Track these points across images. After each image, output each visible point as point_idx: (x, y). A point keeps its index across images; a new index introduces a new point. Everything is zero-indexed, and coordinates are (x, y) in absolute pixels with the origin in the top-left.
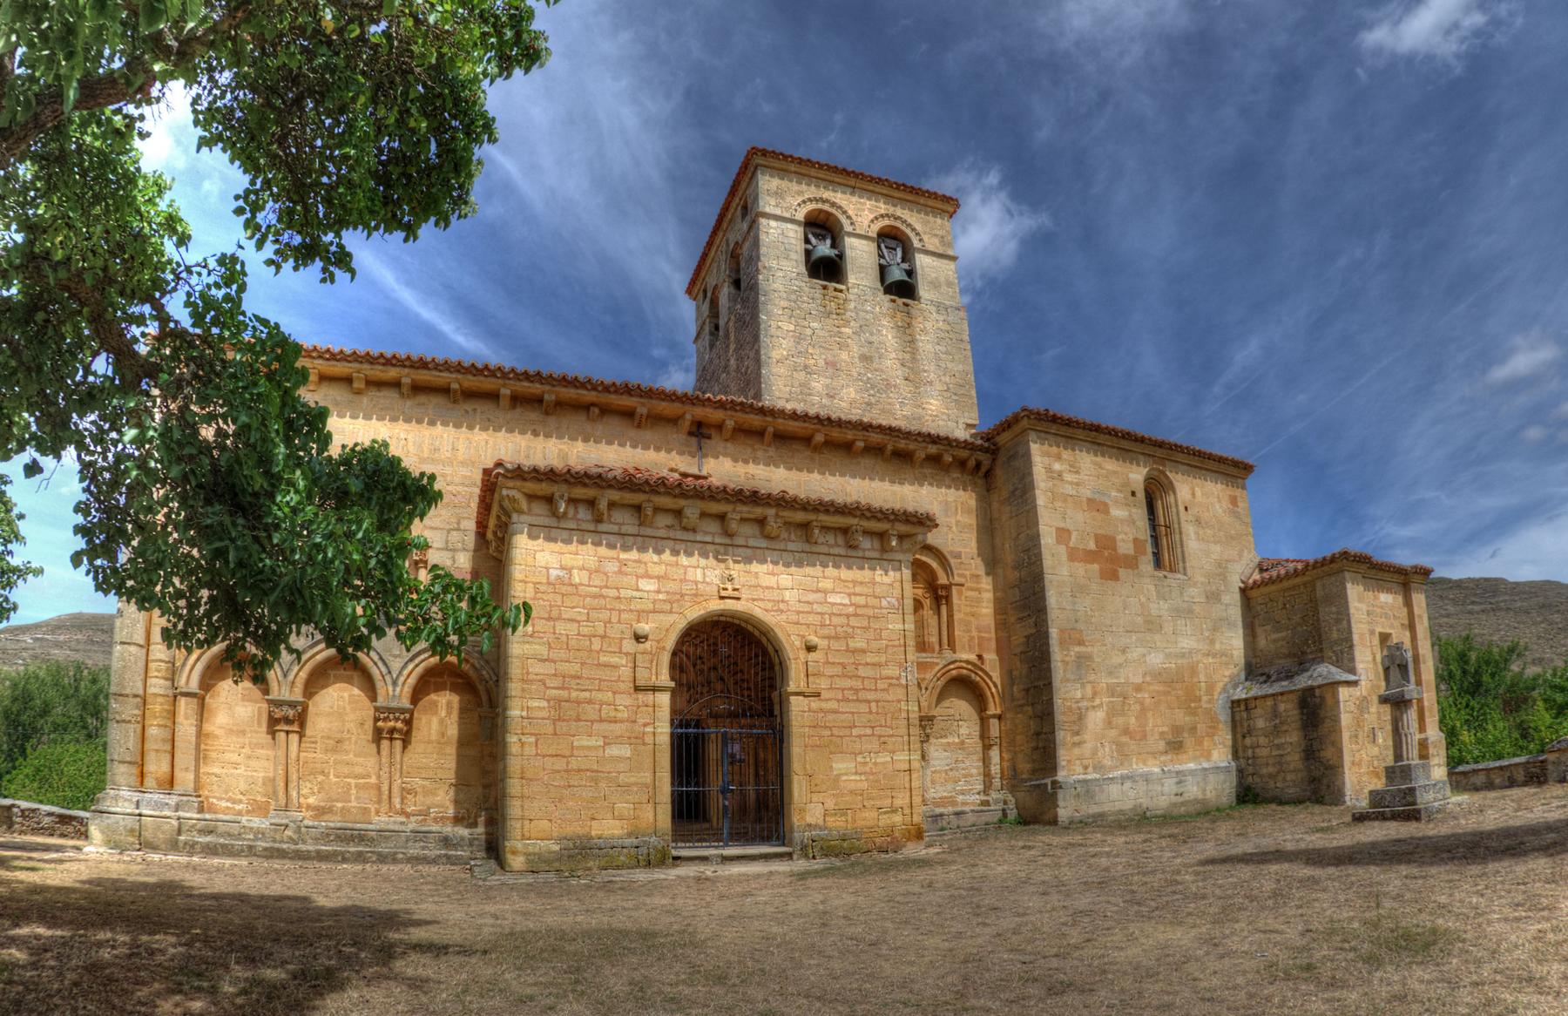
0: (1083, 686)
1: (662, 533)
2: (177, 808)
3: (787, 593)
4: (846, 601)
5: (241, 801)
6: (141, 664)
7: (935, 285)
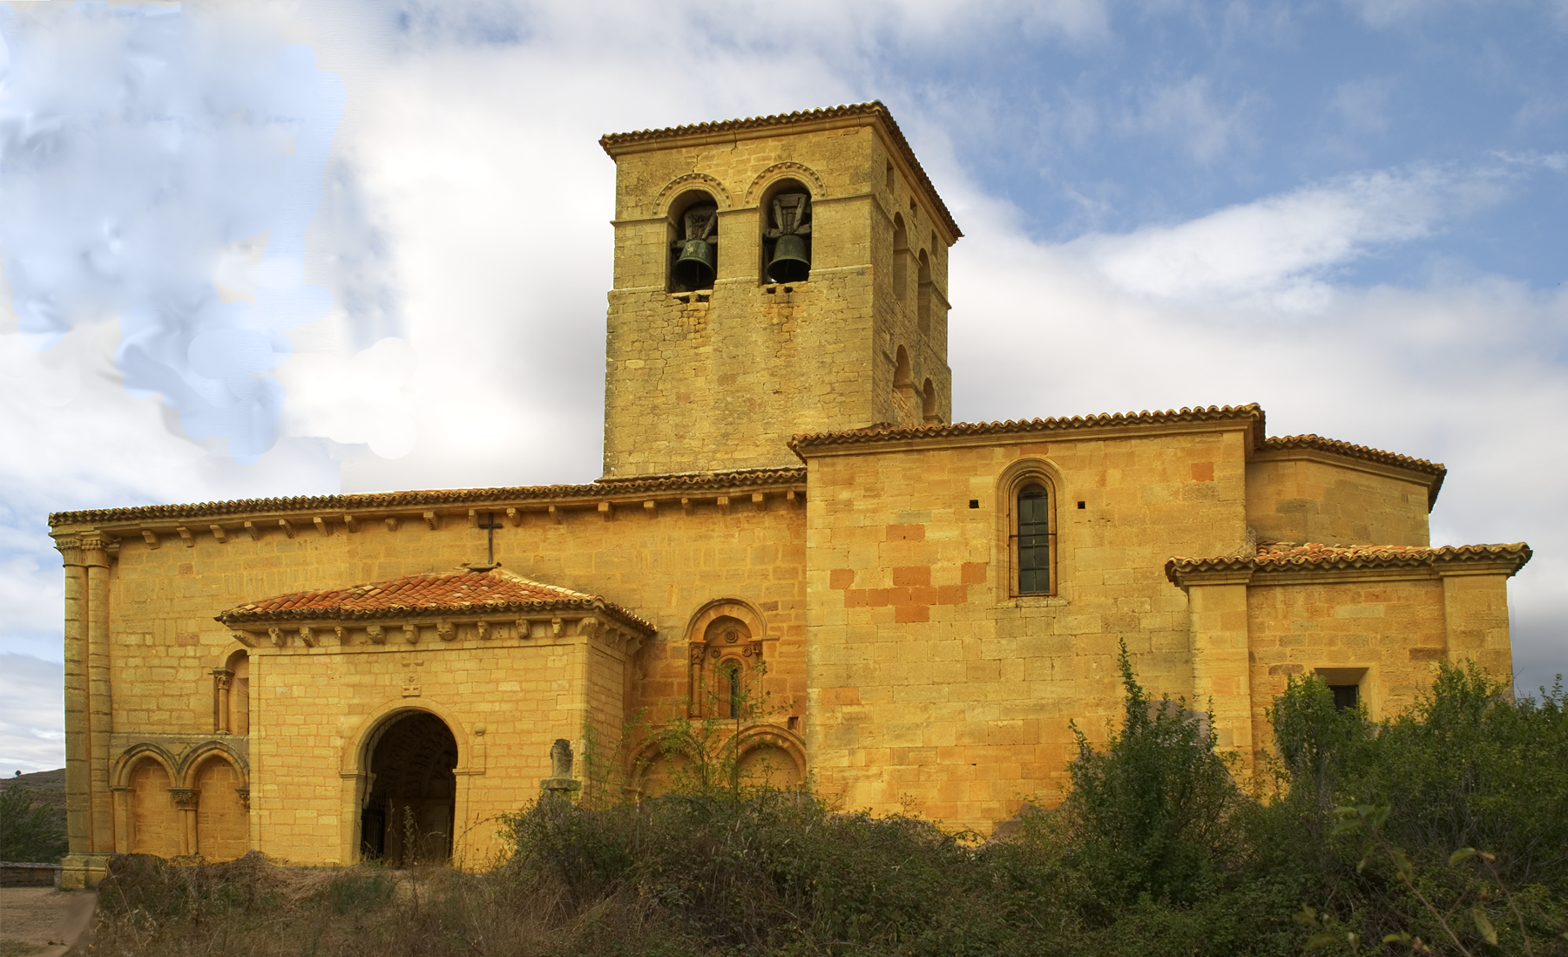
0: (852, 753)
1: (357, 649)
3: (461, 688)
4: (517, 688)
7: (835, 247)
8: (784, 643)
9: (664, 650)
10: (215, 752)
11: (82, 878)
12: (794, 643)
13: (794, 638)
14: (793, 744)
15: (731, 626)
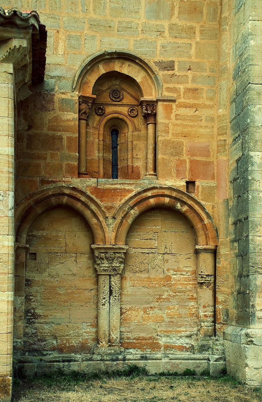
8: (180, 106)
9: (52, 101)
12: (191, 106)
13: (191, 101)
14: (190, 206)
15: (116, 83)
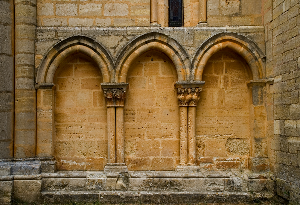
2: (41, 170)
5: (83, 160)
6: (11, 68)
10: (154, 44)
11: (9, 189)
